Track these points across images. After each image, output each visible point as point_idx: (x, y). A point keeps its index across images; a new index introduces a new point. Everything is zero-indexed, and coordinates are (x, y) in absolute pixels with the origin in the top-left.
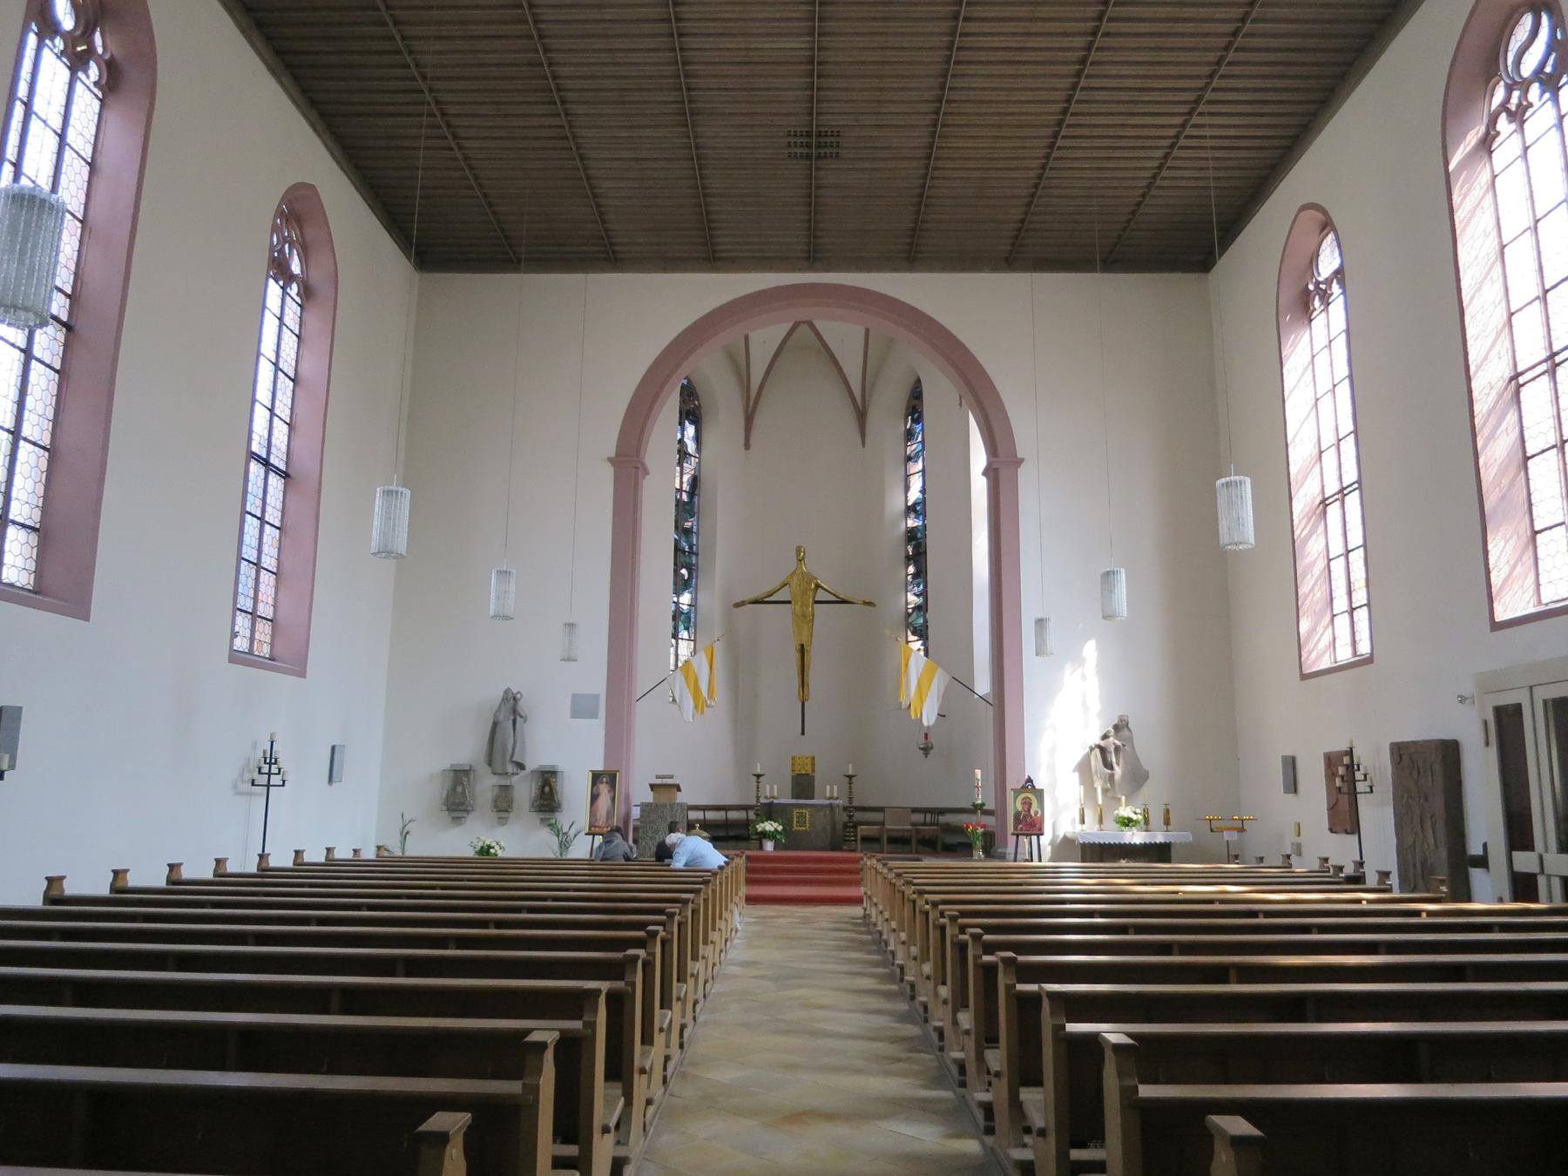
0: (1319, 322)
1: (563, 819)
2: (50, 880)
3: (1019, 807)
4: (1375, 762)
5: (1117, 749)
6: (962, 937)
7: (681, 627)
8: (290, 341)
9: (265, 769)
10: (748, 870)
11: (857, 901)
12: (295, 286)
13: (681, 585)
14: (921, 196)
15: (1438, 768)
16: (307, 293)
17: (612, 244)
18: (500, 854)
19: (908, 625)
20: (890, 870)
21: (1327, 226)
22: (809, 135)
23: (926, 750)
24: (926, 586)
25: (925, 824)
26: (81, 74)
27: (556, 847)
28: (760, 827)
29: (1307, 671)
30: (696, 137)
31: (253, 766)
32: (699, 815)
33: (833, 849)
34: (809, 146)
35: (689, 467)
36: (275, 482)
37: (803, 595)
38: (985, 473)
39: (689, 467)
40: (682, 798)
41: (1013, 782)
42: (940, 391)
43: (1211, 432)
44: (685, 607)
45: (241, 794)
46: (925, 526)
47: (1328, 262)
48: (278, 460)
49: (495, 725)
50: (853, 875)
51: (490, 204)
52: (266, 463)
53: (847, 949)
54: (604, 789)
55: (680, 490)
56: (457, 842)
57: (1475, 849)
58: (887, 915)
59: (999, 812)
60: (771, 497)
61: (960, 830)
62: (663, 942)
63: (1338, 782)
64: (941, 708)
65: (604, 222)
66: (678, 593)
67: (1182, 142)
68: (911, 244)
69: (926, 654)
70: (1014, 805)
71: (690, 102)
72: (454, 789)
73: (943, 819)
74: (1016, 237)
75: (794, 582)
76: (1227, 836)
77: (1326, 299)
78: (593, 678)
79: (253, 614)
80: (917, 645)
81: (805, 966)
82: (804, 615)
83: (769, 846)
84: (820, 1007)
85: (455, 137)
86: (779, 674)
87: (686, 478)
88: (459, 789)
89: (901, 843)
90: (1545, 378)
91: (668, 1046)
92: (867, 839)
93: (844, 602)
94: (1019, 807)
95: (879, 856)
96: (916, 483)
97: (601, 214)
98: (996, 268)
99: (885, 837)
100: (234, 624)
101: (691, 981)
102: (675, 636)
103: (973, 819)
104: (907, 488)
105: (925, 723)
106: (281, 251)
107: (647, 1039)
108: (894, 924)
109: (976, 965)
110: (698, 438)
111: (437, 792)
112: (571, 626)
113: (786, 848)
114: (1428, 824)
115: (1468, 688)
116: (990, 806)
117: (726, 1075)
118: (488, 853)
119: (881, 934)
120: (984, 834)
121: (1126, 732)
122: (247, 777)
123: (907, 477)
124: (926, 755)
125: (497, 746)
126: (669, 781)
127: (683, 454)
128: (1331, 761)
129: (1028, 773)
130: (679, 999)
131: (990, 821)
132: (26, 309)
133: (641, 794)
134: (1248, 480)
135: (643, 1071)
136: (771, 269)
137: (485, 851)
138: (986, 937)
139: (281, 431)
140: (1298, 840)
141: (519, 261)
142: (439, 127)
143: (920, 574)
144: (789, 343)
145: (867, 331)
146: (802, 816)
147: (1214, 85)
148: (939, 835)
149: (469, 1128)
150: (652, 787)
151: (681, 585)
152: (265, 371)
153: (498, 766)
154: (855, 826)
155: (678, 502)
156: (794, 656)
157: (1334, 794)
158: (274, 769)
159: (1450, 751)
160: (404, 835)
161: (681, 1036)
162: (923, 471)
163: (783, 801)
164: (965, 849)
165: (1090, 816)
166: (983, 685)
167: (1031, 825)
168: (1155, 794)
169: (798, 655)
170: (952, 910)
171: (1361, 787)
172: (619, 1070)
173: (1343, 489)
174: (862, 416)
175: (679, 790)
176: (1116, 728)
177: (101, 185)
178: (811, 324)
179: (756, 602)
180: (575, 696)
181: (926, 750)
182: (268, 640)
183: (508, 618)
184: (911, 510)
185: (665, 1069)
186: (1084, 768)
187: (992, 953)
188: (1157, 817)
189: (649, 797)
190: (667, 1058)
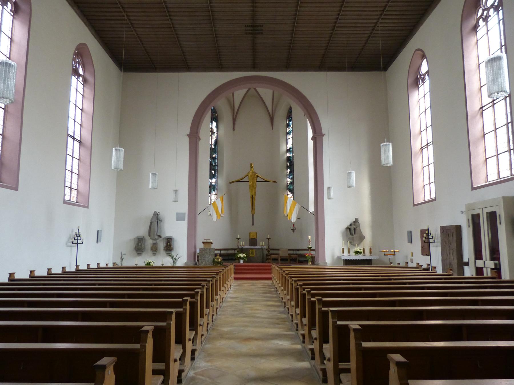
0: (421, 88)
2: (10, 274)
4: (436, 233)
6: (304, 292)
8: (80, 97)
9: (76, 238)
10: (235, 269)
11: (270, 279)
12: (81, 78)
13: (212, 176)
15: (455, 233)
16: (85, 81)
18: (154, 265)
20: (281, 269)
21: (424, 56)
22: (252, 27)
23: (293, 230)
26: (5, 7)
28: (239, 256)
29: (415, 203)
30: (215, 31)
31: (72, 237)
32: (219, 252)
33: (263, 262)
34: (252, 30)
35: (214, 137)
36: (77, 144)
38: (312, 139)
40: (213, 246)
43: (386, 124)
45: (69, 246)
47: (424, 67)
48: (77, 137)
49: (151, 223)
50: (269, 271)
51: (146, 50)
52: (74, 138)
55: (211, 145)
56: (140, 261)
57: (465, 260)
58: (278, 282)
62: (207, 289)
63: (424, 239)
65: (184, 55)
66: (211, 179)
69: (294, 199)
72: (138, 244)
73: (299, 252)
77: (423, 80)
78: (183, 207)
79: (71, 188)
80: (290, 195)
82: (253, 186)
83: (242, 262)
84: (256, 310)
85: (133, 28)
86: (245, 205)
87: (213, 140)
88: (140, 244)
89: (285, 260)
90: (491, 108)
91: (208, 320)
93: (266, 181)
96: (290, 141)
97: (183, 53)
98: (315, 70)
99: (265, 255)
100: (65, 191)
101: (215, 302)
104: (287, 143)
106: (76, 66)
107: (202, 316)
108: (280, 285)
109: (301, 294)
110: (217, 127)
111: (132, 245)
112: (176, 191)
113: (247, 262)
114: (451, 252)
115: (464, 209)
116: (313, 248)
117: (226, 329)
120: (312, 257)
122: (71, 241)
123: (287, 140)
124: (294, 232)
125: (152, 230)
128: (422, 232)
130: (211, 306)
131: (312, 252)
132: (7, 98)
133: (200, 245)
134: (391, 144)
135: (200, 325)
136: (241, 71)
137: (149, 264)
138: (312, 292)
139: (78, 127)
140: (412, 258)
141: (156, 68)
142: (132, 31)
143: (292, 172)
148: (299, 257)
149: (154, 330)
150: (203, 243)
152: (72, 107)
155: (211, 149)
156: (250, 199)
157: (423, 242)
158: (79, 238)
159: (458, 229)
160: (122, 259)
161: (212, 318)
162: (293, 137)
163: (246, 247)
164: (306, 262)
165: (346, 251)
166: (312, 209)
170: (301, 283)
171: (431, 240)
172: (194, 326)
173: (428, 144)
174: (272, 119)
177: (14, 46)
178: (255, 89)
180: (177, 214)
181: (293, 230)
182: (76, 196)
184: (289, 151)
185: (207, 327)
187: (314, 298)
188: (367, 251)
189: (202, 246)
190: (208, 324)
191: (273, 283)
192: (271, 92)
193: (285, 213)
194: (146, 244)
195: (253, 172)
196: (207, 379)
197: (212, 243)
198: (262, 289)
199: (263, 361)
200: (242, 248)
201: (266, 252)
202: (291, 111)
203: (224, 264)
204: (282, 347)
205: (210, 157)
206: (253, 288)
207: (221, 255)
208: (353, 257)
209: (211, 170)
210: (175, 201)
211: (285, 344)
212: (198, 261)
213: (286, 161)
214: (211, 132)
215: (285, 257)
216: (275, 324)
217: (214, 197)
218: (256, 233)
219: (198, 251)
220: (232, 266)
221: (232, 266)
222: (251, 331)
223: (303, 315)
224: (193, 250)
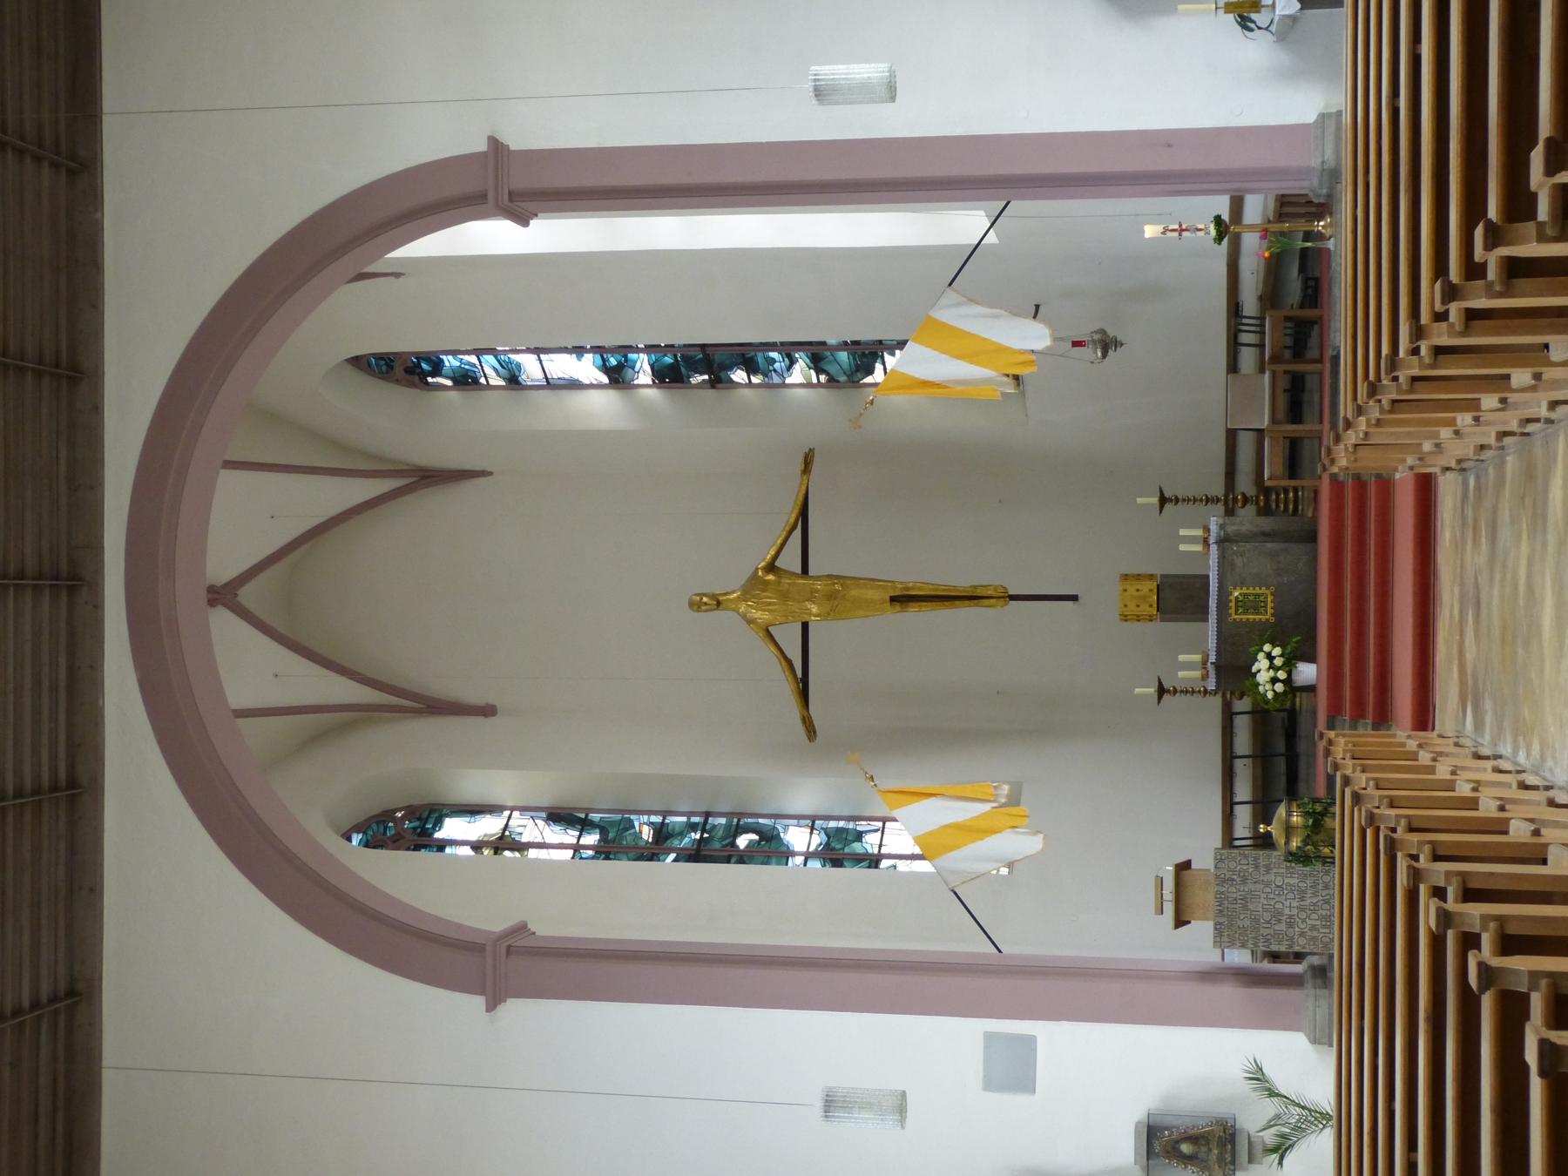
7: (857, 847)
11: (1425, 487)
13: (771, 849)
17: (36, 1005)
20: (1360, 411)
23: (1107, 344)
24: (772, 346)
25: (1261, 346)
33: (1312, 537)
35: (529, 829)
38: (523, 221)
39: (529, 829)
40: (1204, 861)
46: (650, 349)
50: (1368, 496)
55: (577, 848)
61: (1274, 267)
66: (785, 854)
68: (39, 375)
73: (1250, 306)
75: (760, 615)
82: (831, 596)
92: (1293, 465)
95: (1328, 438)
96: (562, 366)
98: (94, 197)
104: (574, 385)
112: (831, 1104)
123: (550, 384)
124: (1117, 344)
133: (1198, 944)
136: (96, 665)
138: (1493, 212)
144: (282, 629)
146: (1245, 605)
148: (1286, 316)
150: (1180, 922)
154: (1267, 491)
155: (605, 851)
156: (915, 616)
162: (538, 351)
163: (1212, 643)
166: (963, 224)
174: (428, 478)
179: (804, 694)
180: (990, 1084)
181: (1107, 344)
184: (618, 376)
187: (1533, 198)
189: (1201, 930)
191: (1461, 467)
192: (227, 478)
195: (744, 597)
197: (1183, 867)
198: (1505, 534)
200: (1218, 667)
201: (1247, 518)
202: (380, 357)
203: (1321, 792)
205: (652, 857)
206: (1494, 598)
207: (1263, 811)
209: (729, 855)
212: (1298, 957)
213: (679, 393)
214: (508, 850)
215: (1282, 400)
217: (898, 839)
218: (1125, 577)
219: (1239, 957)
220: (1341, 744)
221: (1341, 744)
224: (1231, 993)
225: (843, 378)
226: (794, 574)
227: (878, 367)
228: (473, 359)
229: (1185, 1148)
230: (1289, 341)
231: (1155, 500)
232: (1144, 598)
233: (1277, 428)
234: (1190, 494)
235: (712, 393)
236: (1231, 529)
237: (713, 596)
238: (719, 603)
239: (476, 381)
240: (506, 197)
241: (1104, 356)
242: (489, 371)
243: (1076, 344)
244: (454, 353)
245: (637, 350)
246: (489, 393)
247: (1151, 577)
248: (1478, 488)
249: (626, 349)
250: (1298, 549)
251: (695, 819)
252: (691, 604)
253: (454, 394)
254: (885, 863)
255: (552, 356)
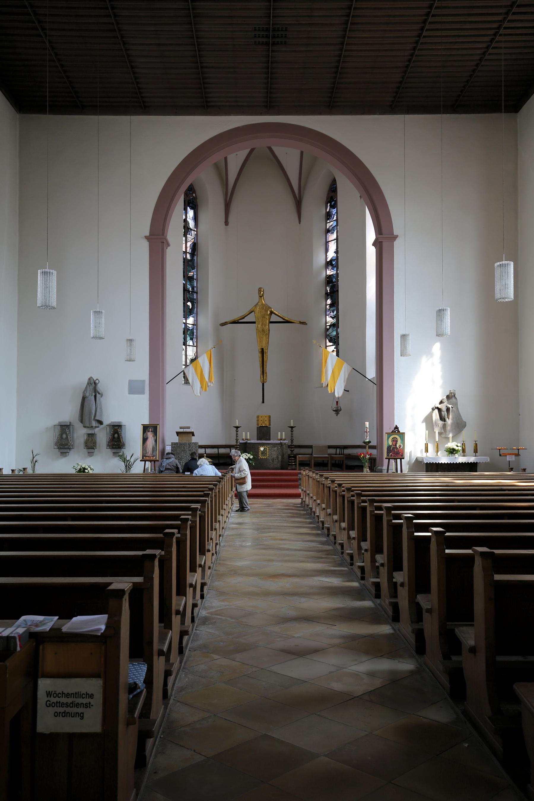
1: (127, 452)
3: (390, 443)
5: (448, 409)
7: (188, 338)
11: (298, 496)
13: (188, 312)
14: (337, 67)
17: (142, 97)
18: (91, 472)
19: (327, 336)
22: (268, 30)
24: (338, 312)
27: (123, 468)
33: (282, 469)
34: (267, 37)
37: (262, 318)
38: (374, 245)
40: (194, 439)
41: (387, 428)
42: (348, 192)
44: (190, 326)
46: (337, 274)
49: (84, 399)
50: (295, 483)
53: (292, 517)
54: (150, 435)
55: (185, 252)
56: (65, 466)
58: (315, 498)
59: (378, 447)
60: (243, 254)
61: (357, 458)
64: (345, 387)
66: (186, 317)
67: (502, 31)
69: (338, 355)
70: (387, 442)
71: (193, 9)
72: (61, 435)
73: (347, 451)
74: (397, 92)
76: (508, 458)
78: (142, 371)
80: (331, 348)
81: (271, 524)
82: (263, 330)
84: (281, 540)
87: (189, 244)
88: (64, 436)
89: (321, 465)
93: (288, 322)
94: (390, 443)
96: (332, 247)
97: (136, 78)
102: (185, 344)
103: (364, 451)
104: (327, 250)
105: (337, 395)
109: (358, 507)
110: (196, 218)
111: (52, 437)
112: (130, 341)
118: (84, 472)
119: (311, 509)
120: (370, 459)
121: (453, 399)
123: (327, 243)
124: (337, 414)
126: (188, 430)
127: (187, 229)
129: (396, 423)
131: (374, 452)
133: (170, 438)
143: (335, 304)
145: (302, 153)
147: (509, 18)
148: (345, 460)
150: (178, 433)
151: (188, 312)
153: (86, 422)
154: (295, 457)
155: (185, 260)
156: (258, 355)
160: (34, 463)
162: (337, 239)
163: (252, 441)
164: (360, 468)
165: (431, 447)
166: (371, 373)
167: (396, 453)
168: (469, 436)
169: (260, 355)
174: (298, 204)
175: (193, 435)
176: (448, 397)
180: (130, 381)
181: (337, 411)
183: (101, 338)
184: (329, 264)
186: (428, 420)
188: (470, 448)
189: (176, 439)
192: (297, 153)
193: (324, 381)
194: (75, 435)
196: (228, 619)
199: (303, 600)
200: (246, 443)
202: (336, 188)
204: (330, 585)
205: (184, 276)
208: (444, 459)
210: (130, 360)
211: (335, 581)
216: (316, 559)
218: (270, 417)
222: (278, 567)
223: (362, 537)
225: (328, 333)
226: (270, 319)
227: (331, 344)
228: (335, 218)
229: (116, 435)
230: (337, 462)
231: (292, 425)
232: (264, 422)
233: (313, 458)
234: (294, 435)
235: (324, 293)
236: (284, 446)
237: (263, 295)
238: (261, 297)
239: (328, 219)
240: (380, 241)
241: (334, 410)
242: (331, 223)
243: (337, 402)
244: (337, 212)
245: (337, 271)
246: (325, 223)
247: (270, 424)
248: (297, 507)
249: (337, 267)
250: (279, 465)
251: (195, 289)
252: (260, 288)
253: (324, 212)
254: (184, 347)
255: (335, 244)
